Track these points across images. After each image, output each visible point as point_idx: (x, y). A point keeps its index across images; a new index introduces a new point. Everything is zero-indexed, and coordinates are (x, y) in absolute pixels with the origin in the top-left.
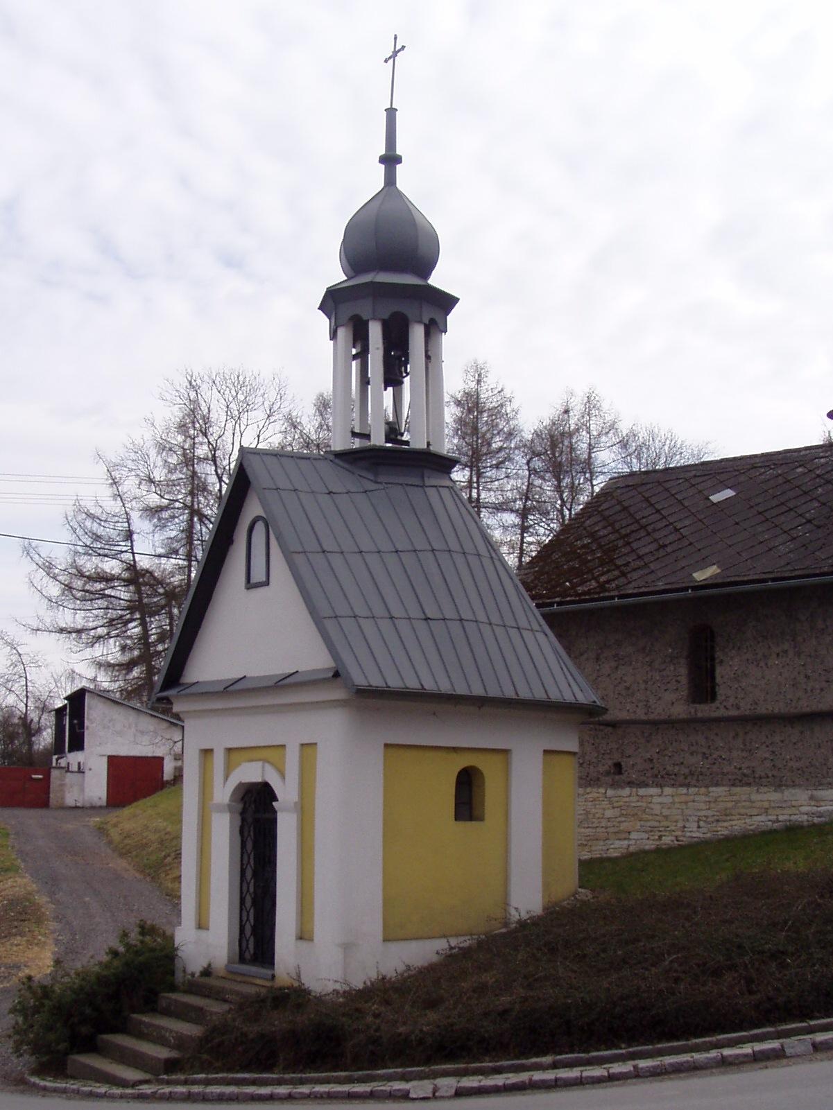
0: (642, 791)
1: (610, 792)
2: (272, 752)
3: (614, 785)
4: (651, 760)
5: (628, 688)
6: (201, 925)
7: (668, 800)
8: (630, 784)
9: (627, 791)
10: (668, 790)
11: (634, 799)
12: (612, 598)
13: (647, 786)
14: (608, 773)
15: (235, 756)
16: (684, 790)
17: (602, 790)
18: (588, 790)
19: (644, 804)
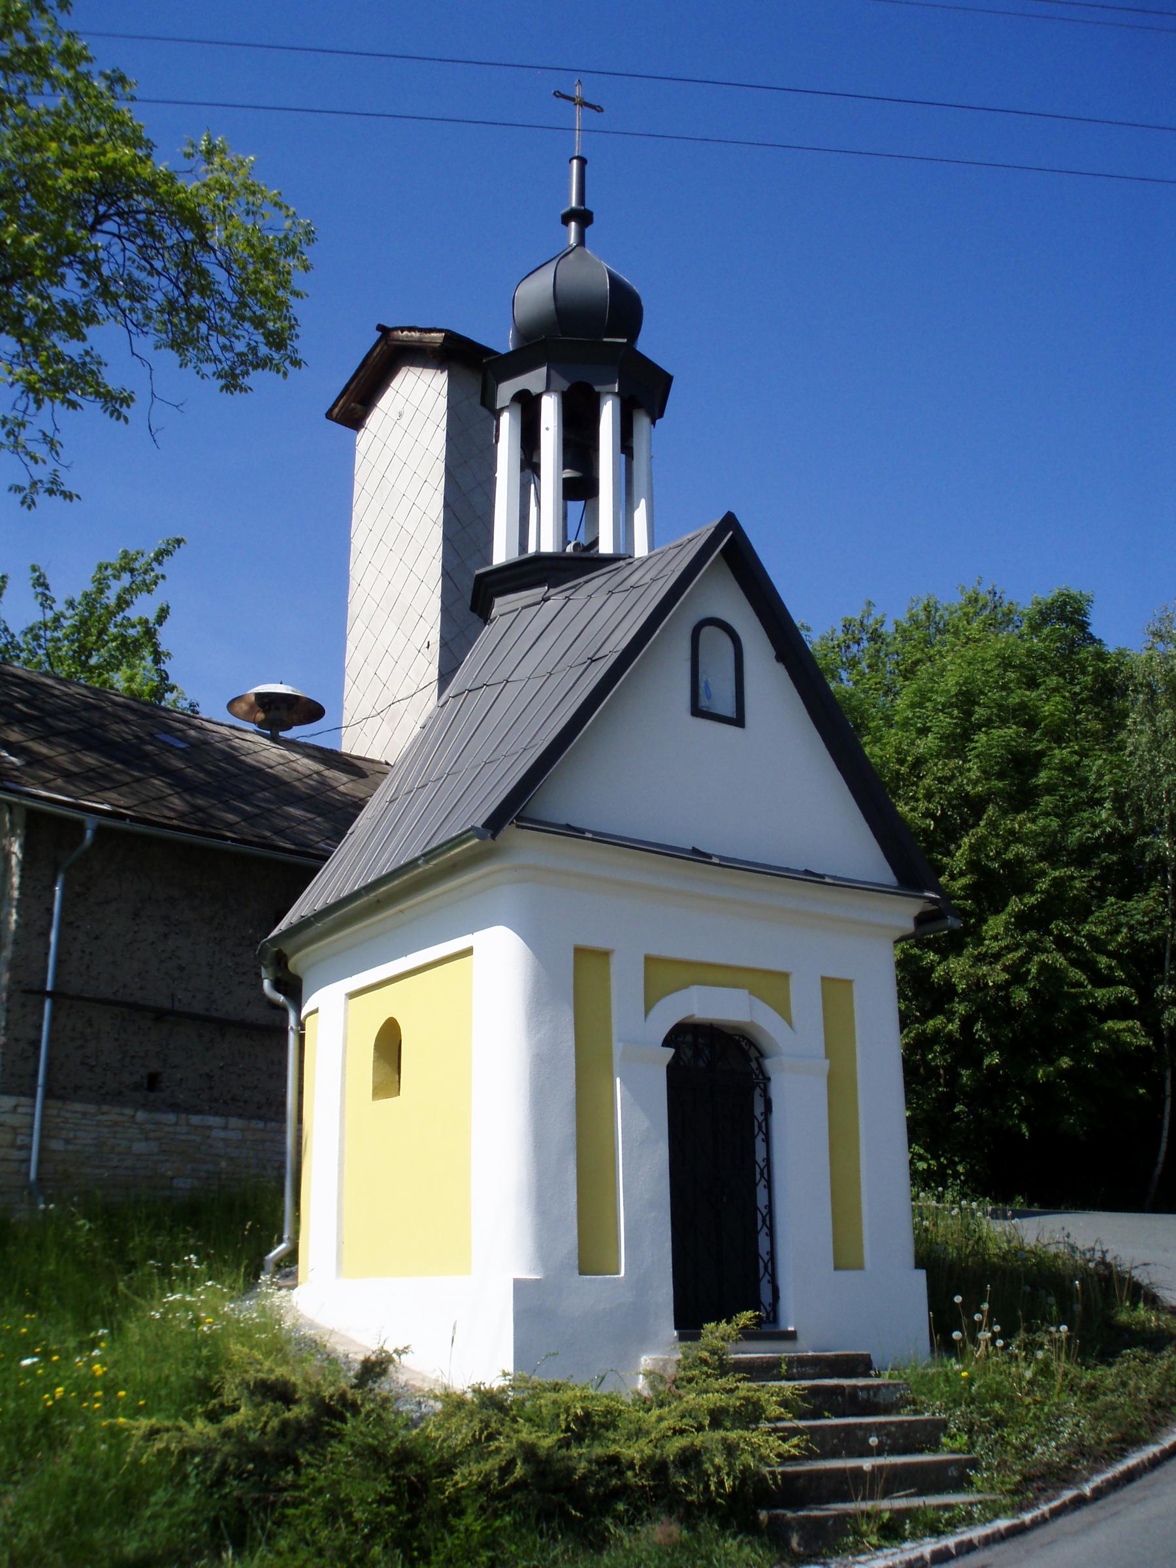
0: (195, 1119)
1: (141, 1116)
2: (771, 985)
3: (145, 1106)
4: (210, 1077)
5: (181, 969)
6: (846, 1257)
7: (234, 1135)
8: (174, 1107)
9: (171, 1118)
10: (234, 1122)
11: (184, 1129)
12: (226, 838)
13: (199, 1112)
14: (137, 1087)
15: (704, 702)
16: (261, 1125)
17: (128, 1111)
18: (105, 1108)
19: (198, 1139)
